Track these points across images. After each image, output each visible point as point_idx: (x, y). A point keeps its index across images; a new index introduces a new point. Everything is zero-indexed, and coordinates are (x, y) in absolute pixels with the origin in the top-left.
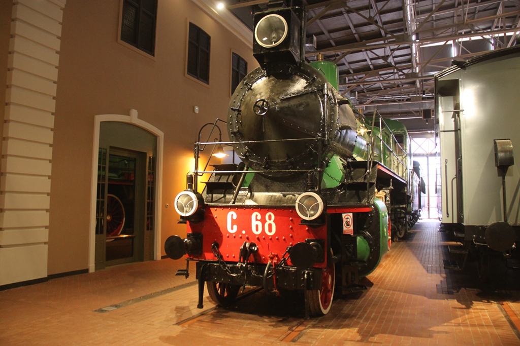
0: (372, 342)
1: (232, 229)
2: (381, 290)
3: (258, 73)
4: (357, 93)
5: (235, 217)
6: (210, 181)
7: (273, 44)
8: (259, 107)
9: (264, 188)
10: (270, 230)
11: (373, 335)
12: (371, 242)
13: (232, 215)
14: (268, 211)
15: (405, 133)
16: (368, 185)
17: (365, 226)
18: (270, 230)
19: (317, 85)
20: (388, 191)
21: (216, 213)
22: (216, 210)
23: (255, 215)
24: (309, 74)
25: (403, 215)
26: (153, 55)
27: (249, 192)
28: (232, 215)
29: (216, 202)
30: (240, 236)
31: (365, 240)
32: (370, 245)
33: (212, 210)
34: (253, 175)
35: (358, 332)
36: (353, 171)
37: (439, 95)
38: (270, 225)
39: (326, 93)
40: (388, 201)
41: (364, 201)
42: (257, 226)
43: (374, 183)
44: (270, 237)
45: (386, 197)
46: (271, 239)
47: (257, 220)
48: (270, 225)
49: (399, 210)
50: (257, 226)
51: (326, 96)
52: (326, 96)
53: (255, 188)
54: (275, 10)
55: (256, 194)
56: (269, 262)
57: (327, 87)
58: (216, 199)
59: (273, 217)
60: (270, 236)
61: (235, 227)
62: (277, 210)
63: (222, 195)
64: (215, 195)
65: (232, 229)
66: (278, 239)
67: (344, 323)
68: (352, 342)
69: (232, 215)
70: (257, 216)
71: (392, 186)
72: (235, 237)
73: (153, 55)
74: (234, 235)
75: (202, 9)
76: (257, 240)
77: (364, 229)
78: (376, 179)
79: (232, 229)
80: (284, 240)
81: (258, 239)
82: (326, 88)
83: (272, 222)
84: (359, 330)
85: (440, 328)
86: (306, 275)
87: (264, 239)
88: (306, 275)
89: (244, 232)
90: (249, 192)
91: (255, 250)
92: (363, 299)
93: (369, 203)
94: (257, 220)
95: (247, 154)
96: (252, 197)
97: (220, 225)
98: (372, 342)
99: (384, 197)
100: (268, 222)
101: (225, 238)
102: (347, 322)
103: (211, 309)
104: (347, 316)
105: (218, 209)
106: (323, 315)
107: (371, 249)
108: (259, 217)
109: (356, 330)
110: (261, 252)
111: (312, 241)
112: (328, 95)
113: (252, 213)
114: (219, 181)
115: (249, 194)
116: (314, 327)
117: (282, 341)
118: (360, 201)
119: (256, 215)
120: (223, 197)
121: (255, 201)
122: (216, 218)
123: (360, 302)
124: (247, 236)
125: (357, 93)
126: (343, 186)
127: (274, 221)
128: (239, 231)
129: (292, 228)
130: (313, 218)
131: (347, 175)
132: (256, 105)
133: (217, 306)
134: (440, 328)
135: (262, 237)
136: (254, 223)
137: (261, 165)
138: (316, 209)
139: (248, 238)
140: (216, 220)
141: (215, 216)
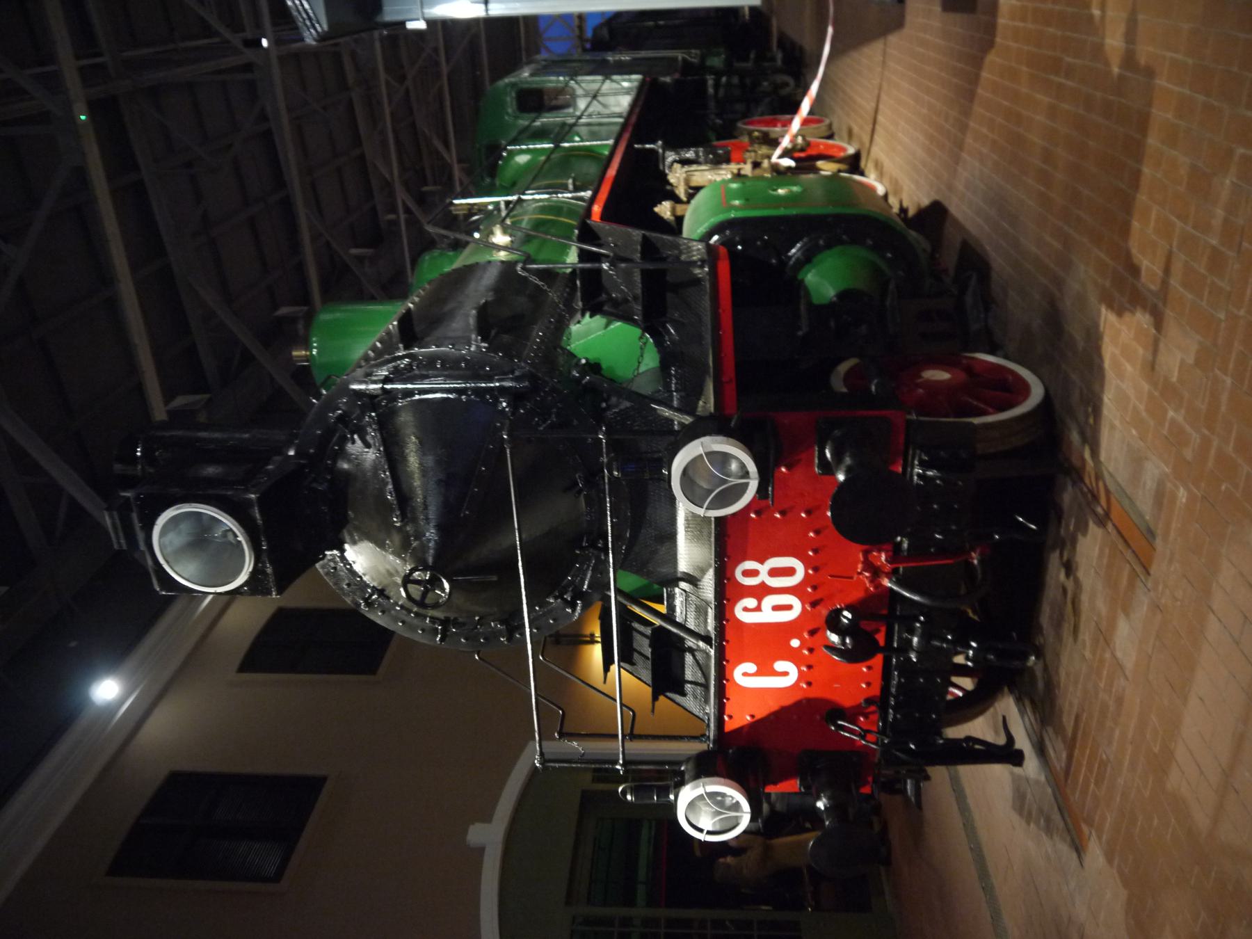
0: (1165, 283)
1: (785, 674)
2: (960, 186)
3: (335, 568)
4: (425, 189)
5: (750, 667)
6: (650, 682)
7: (240, 538)
8: (424, 594)
9: (663, 550)
10: (790, 572)
11: (1135, 270)
12: (821, 242)
13: (744, 675)
14: (732, 578)
15: (513, 85)
16: (650, 266)
17: (774, 261)
18: (790, 572)
19: (358, 412)
20: (671, 157)
21: (740, 716)
22: (730, 717)
23: (745, 613)
24: (330, 431)
25: (735, 80)
26: (323, 780)
27: (678, 586)
28: (745, 674)
29: (706, 676)
30: (806, 652)
31: (815, 260)
32: (829, 246)
33: (730, 726)
34: (620, 572)
35: (1120, 314)
36: (609, 295)
37: (379, 19)
38: (774, 573)
39: (380, 386)
40: (697, 153)
41: (702, 272)
42: (776, 608)
43: (644, 237)
44: (811, 572)
45: (685, 162)
46: (816, 569)
47: (758, 609)
48: (774, 573)
49: (721, 92)
50: (776, 608)
51: (388, 387)
52: (388, 387)
53: (664, 570)
54: (141, 536)
55: (683, 566)
56: (887, 583)
57: (361, 382)
58: (700, 674)
59: (750, 565)
60: (806, 574)
61: (780, 666)
62: (728, 637)
63: (689, 658)
64: (689, 675)
65: (785, 674)
66: (815, 551)
67: (1081, 345)
68: (1162, 346)
69: (745, 674)
70: (746, 609)
71: (654, 142)
72: (809, 667)
73: (323, 780)
74: (805, 669)
75: (204, 637)
76: (819, 607)
77: (783, 263)
78: (630, 230)
79: (786, 675)
80: (817, 532)
81: (814, 604)
82: (363, 387)
83: (764, 569)
84: (1110, 307)
85: (1114, 42)
86: (930, 473)
87: (814, 588)
88: (930, 473)
89: (795, 643)
90: (678, 586)
91: (850, 616)
92: (988, 248)
93: (703, 261)
94: (758, 609)
95: (568, 597)
96: (693, 580)
97: (772, 706)
98: (1165, 283)
99: (686, 168)
100: (763, 577)
101: (815, 693)
102: (1075, 331)
103: (1022, 717)
104: (1054, 320)
105: (728, 710)
106: (1047, 400)
107: (842, 243)
108: (751, 602)
109: (1107, 318)
110: (856, 595)
111: (822, 455)
112: (386, 380)
113: (738, 620)
114: (647, 658)
115: (683, 585)
116: (1092, 439)
117: (1148, 573)
118: (697, 281)
119: (745, 612)
120: (694, 656)
121: (703, 571)
122: (752, 716)
123: (998, 263)
124: (806, 635)
125: (425, 189)
126: (652, 325)
127: (762, 562)
128: (793, 656)
129: (782, 513)
130: (752, 467)
131: (618, 311)
132: (421, 604)
133: (1011, 692)
134: (1114, 42)
135: (809, 592)
136: (767, 615)
137: (598, 558)
138: (722, 460)
139: (812, 633)
140: (759, 716)
141: (748, 718)
